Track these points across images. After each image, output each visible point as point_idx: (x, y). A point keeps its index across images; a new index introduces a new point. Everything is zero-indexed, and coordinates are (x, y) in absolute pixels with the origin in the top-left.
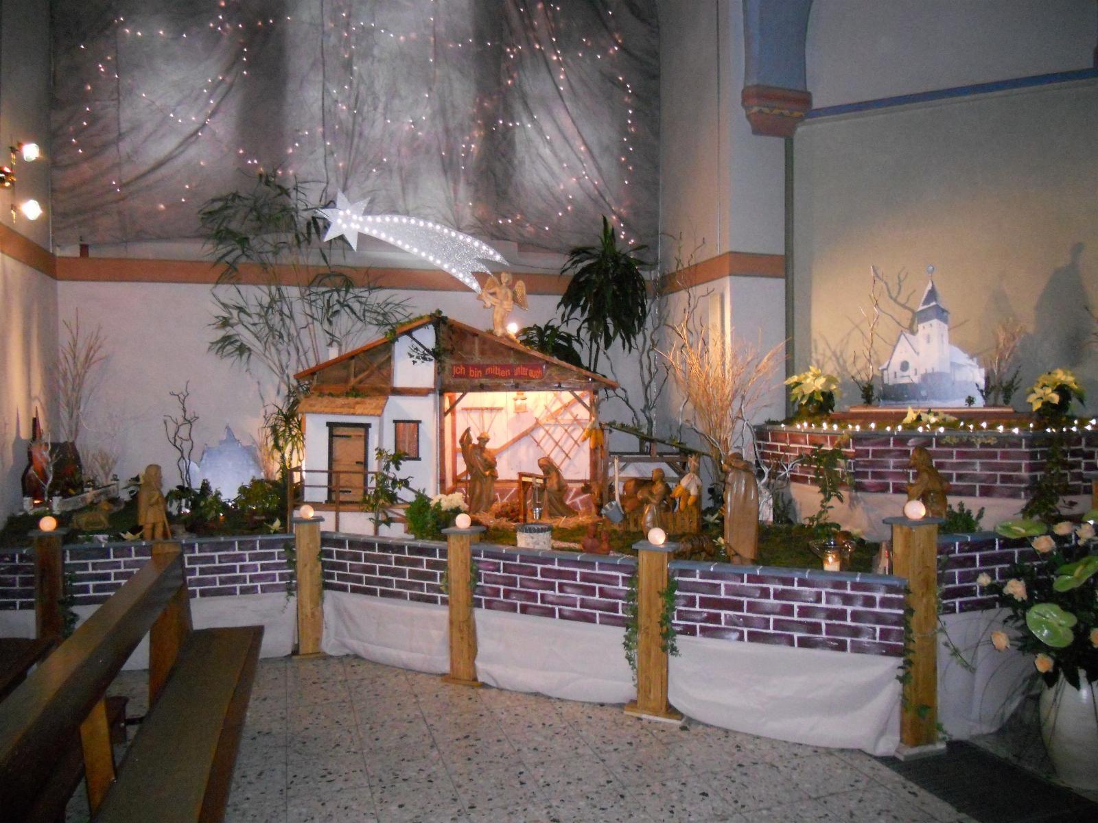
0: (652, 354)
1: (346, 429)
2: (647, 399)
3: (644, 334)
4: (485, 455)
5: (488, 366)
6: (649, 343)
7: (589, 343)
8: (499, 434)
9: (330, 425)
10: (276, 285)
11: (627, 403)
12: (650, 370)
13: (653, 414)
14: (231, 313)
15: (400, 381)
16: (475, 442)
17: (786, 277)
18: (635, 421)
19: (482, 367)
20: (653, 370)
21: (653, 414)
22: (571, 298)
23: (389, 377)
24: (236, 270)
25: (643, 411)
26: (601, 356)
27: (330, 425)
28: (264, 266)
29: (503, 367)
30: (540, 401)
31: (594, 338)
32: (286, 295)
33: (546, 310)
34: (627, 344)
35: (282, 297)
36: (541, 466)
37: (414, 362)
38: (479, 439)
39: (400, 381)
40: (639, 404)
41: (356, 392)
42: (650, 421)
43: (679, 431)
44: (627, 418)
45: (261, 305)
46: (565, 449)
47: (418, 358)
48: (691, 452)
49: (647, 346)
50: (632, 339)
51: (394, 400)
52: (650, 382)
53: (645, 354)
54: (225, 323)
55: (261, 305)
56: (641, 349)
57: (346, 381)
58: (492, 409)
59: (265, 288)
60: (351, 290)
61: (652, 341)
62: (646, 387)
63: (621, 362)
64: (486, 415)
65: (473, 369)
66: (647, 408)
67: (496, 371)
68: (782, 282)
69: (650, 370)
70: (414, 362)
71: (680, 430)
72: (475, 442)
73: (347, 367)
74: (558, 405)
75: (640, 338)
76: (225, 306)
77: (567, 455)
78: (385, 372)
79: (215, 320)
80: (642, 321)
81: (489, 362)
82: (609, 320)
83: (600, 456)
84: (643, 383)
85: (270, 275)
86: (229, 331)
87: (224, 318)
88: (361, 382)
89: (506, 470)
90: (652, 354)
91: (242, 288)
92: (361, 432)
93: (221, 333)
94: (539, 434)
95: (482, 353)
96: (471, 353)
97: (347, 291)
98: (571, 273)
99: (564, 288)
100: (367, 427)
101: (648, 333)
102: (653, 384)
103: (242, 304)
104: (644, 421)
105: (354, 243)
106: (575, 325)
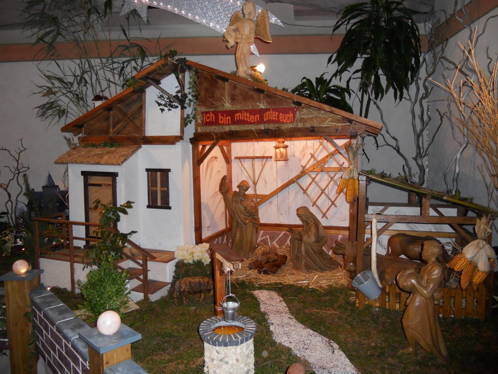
0: (424, 101)
1: (98, 178)
2: (418, 147)
3: (417, 84)
4: (245, 203)
5: (236, 112)
6: (422, 91)
7: (360, 94)
8: (269, 178)
9: (83, 173)
10: (87, 58)
11: (398, 151)
12: (422, 118)
13: (425, 162)
14: (53, 84)
15: (151, 131)
16: (235, 188)
17: (421, 207)
18: (406, 169)
19: (231, 113)
20: (425, 118)
21: (425, 162)
22: (345, 57)
23: (141, 127)
24: (54, 48)
25: (415, 159)
26: (372, 106)
27: (83, 173)
28: (77, 42)
29: (253, 112)
30: (303, 150)
31: (364, 88)
32: (94, 65)
33: (318, 66)
34: (398, 93)
35: (91, 66)
36: (298, 215)
37: (162, 110)
38: (239, 187)
39: (151, 131)
40: (410, 151)
41: (114, 142)
42: (422, 169)
43: (456, 179)
44: (393, 167)
45: (75, 76)
46: (331, 197)
47: (165, 105)
48: (481, 212)
49: (420, 96)
50: (405, 91)
51: (145, 148)
52: (422, 131)
53: (418, 103)
54: (50, 92)
55: (75, 76)
56: (413, 99)
57: (107, 132)
58: (263, 158)
59: (78, 61)
60: (146, 59)
61: (426, 88)
62: (418, 136)
63: (394, 113)
64: (258, 164)
65: (222, 115)
66: (419, 155)
67: (245, 116)
68: (419, 208)
69: (422, 118)
70: (162, 110)
71: (456, 179)
72: (235, 188)
73: (107, 118)
74: (324, 154)
75: (413, 88)
76: (49, 77)
77: (333, 203)
78: (137, 122)
79: (38, 90)
80: (415, 70)
81: (238, 107)
82: (380, 72)
83: (359, 206)
84: (415, 131)
85: (82, 51)
86: (53, 98)
87: (48, 87)
88: (119, 132)
89: (268, 214)
90: (424, 101)
91: (60, 62)
92: (109, 180)
93: (46, 100)
94: (305, 181)
95: (233, 98)
96: (220, 100)
97: (143, 60)
98: (343, 30)
99: (337, 46)
100: (114, 176)
101: (421, 83)
102: (425, 133)
103: (60, 75)
104: (415, 170)
105: (144, 15)
106: (352, 79)
